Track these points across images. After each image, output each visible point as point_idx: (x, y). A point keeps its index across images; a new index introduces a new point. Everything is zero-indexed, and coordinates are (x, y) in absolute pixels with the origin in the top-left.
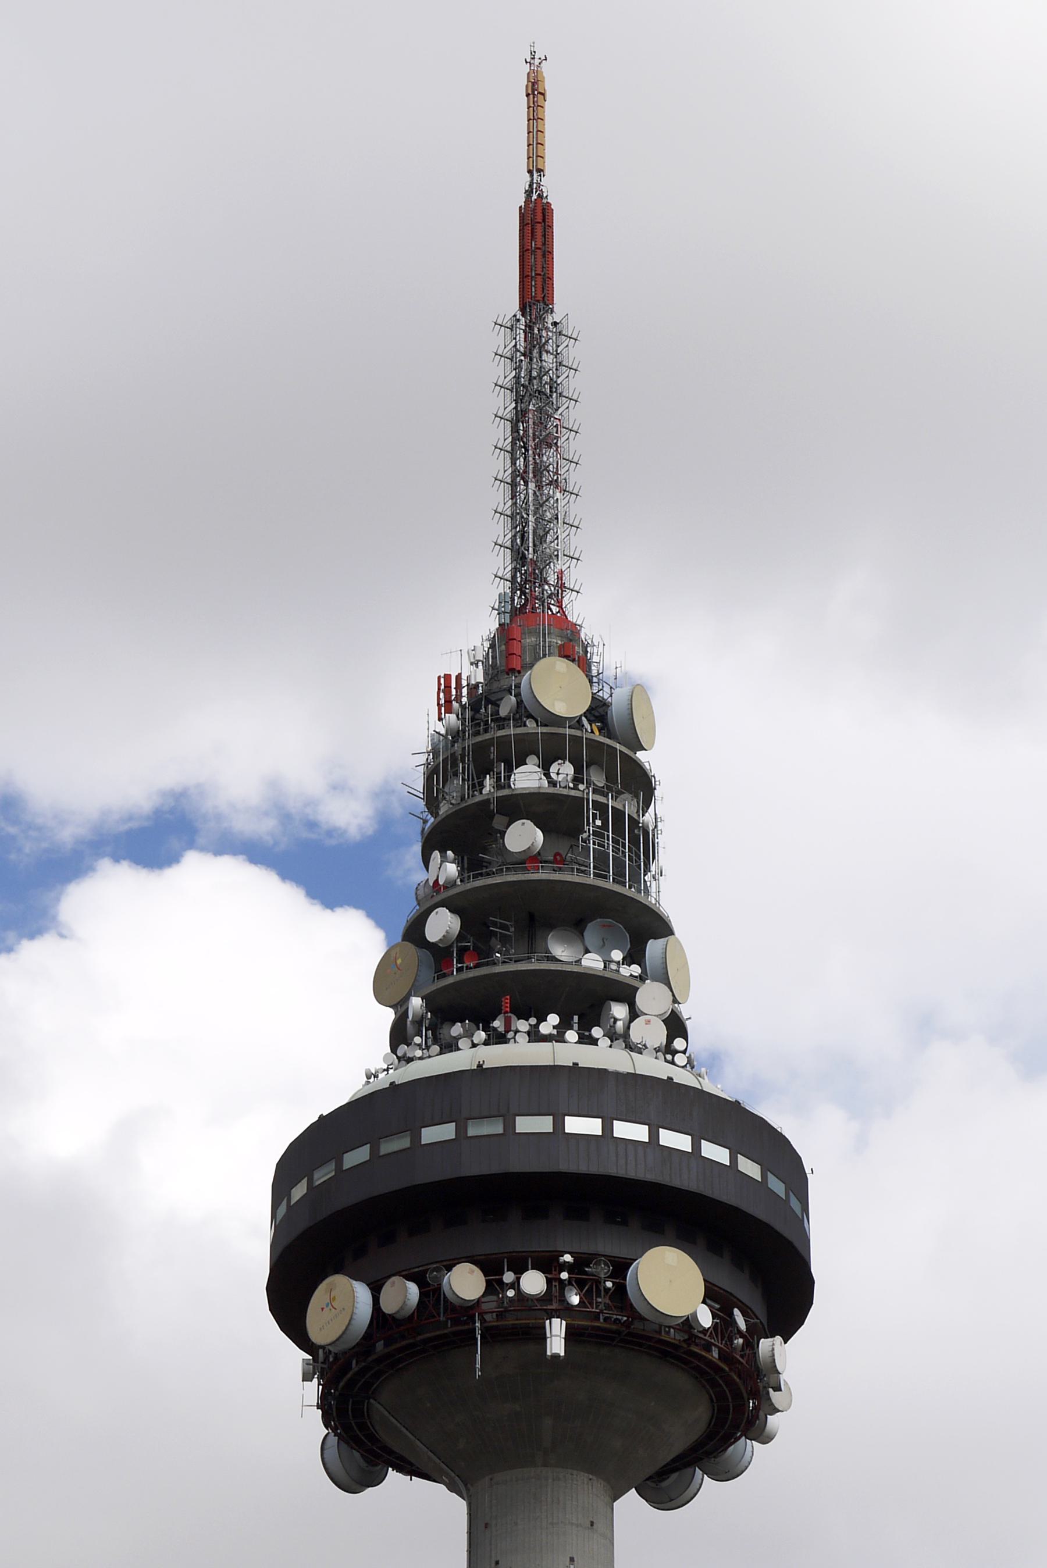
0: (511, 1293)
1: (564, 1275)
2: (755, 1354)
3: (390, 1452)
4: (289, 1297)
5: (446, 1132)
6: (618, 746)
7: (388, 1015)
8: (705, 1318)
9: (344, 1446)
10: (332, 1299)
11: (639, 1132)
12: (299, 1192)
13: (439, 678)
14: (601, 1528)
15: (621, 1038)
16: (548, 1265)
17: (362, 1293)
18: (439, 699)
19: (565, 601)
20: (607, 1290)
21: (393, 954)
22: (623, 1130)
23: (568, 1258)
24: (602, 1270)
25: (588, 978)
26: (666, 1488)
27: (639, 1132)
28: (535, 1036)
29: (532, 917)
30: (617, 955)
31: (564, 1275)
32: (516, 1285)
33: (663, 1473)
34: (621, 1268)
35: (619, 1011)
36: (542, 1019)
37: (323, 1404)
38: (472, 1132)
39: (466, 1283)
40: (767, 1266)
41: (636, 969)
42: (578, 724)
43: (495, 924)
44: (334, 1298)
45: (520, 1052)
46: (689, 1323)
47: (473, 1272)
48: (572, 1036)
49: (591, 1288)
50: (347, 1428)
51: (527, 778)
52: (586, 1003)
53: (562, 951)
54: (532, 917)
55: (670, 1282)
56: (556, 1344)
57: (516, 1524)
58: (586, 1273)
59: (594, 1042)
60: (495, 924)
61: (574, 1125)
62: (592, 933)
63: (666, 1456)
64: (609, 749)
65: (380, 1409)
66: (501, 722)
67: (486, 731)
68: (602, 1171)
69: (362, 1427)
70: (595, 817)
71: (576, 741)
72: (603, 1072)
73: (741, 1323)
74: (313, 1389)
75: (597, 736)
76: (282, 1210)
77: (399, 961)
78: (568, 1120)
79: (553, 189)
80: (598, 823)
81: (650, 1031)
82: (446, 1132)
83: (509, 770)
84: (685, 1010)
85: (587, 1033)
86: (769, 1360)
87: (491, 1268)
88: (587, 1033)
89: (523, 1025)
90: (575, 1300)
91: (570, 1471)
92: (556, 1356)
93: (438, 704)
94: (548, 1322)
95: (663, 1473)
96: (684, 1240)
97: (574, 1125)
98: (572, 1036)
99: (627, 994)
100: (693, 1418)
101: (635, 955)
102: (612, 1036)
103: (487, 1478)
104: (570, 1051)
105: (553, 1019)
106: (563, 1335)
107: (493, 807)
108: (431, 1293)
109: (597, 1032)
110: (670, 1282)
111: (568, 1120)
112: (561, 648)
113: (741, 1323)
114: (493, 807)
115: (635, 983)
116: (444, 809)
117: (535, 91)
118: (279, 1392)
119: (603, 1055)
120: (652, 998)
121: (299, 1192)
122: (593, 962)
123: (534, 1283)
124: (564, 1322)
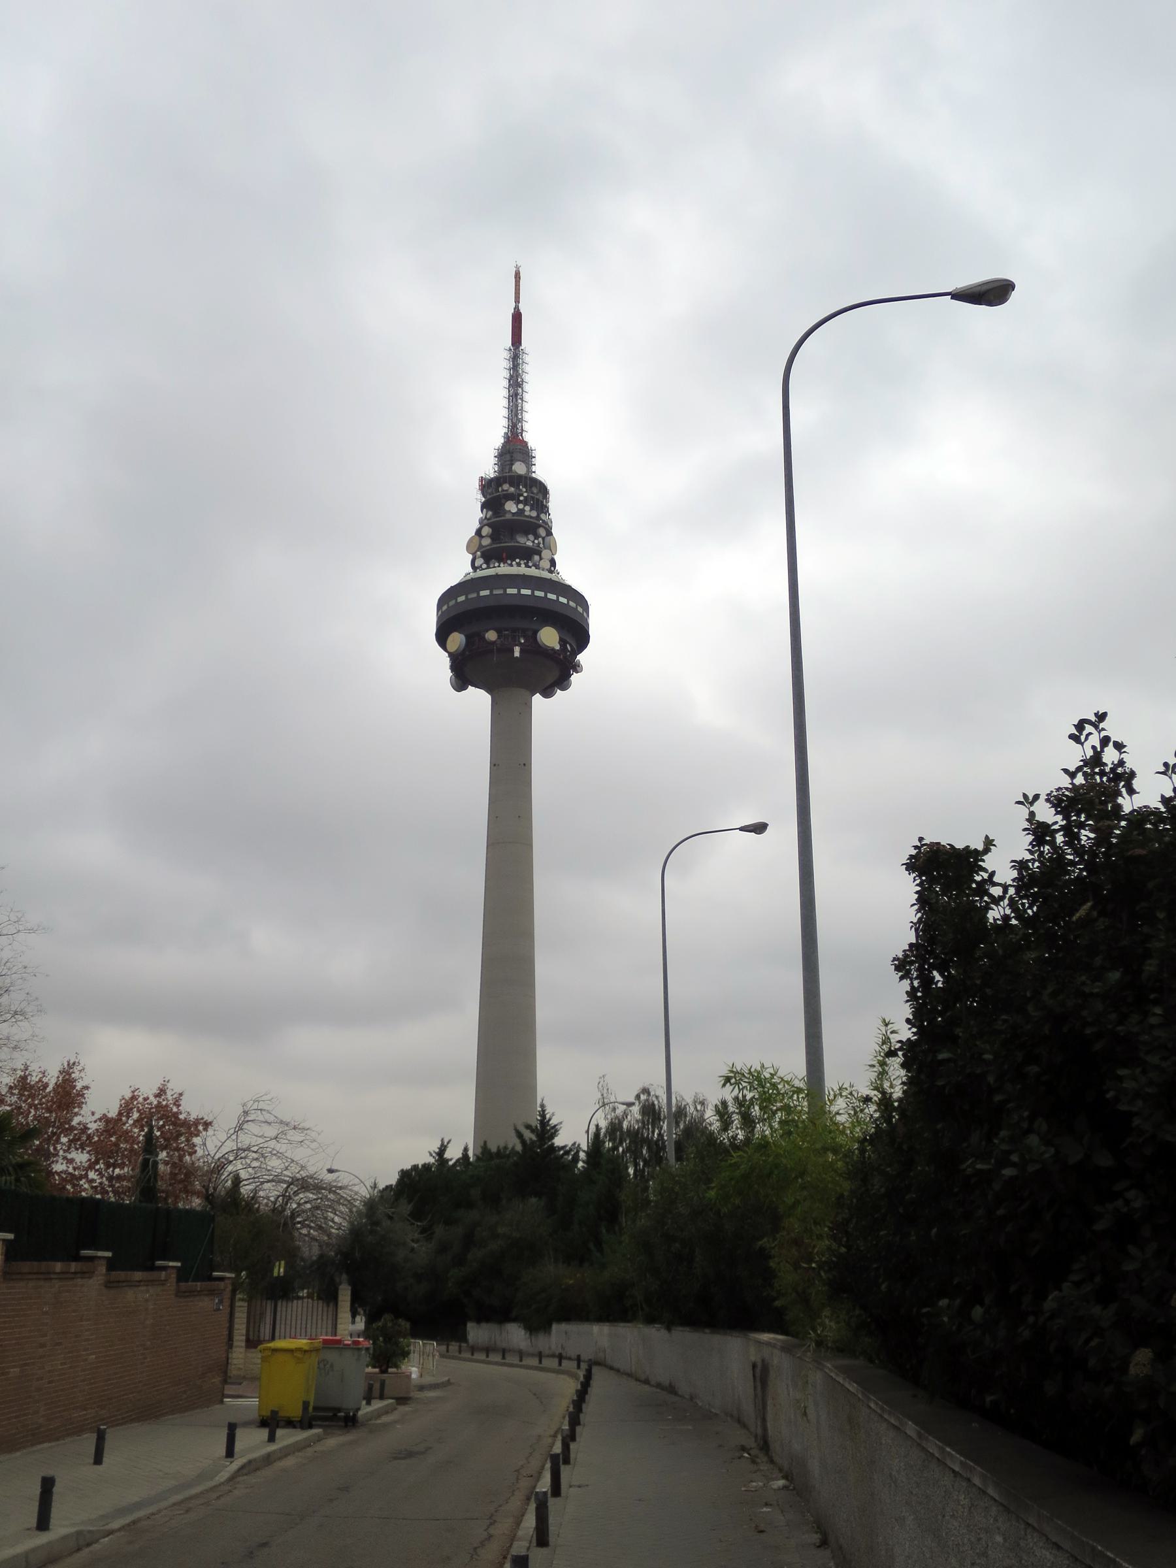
4: (442, 637)
7: (471, 557)
11: (528, 592)
12: (445, 608)
14: (528, 706)
15: (537, 567)
22: (523, 592)
25: (528, 548)
26: (547, 693)
27: (528, 592)
33: (546, 688)
34: (536, 632)
35: (536, 558)
40: (577, 633)
46: (553, 649)
52: (527, 555)
55: (549, 637)
56: (517, 653)
61: (509, 591)
64: (538, 493)
79: (532, 436)
81: (545, 564)
84: (556, 557)
95: (546, 688)
96: (553, 625)
97: (509, 591)
99: (539, 553)
100: (554, 675)
110: (549, 637)
117: (517, 276)
118: (441, 662)
120: (546, 554)
121: (445, 608)
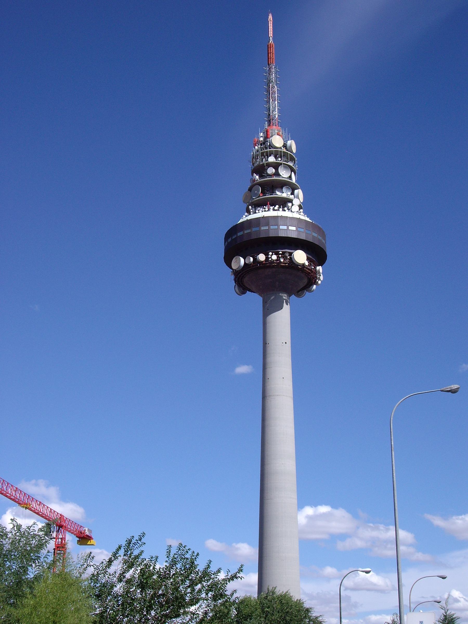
0: (270, 259)
1: (280, 256)
2: (316, 270)
3: (247, 287)
6: (289, 152)
8: (307, 264)
12: (229, 240)
16: (277, 254)
17: (242, 260)
23: (281, 252)
24: (287, 255)
29: (273, 186)
30: (289, 193)
31: (280, 256)
32: (271, 258)
34: (291, 254)
35: (290, 204)
36: (275, 206)
37: (235, 280)
39: (262, 257)
41: (293, 196)
42: (280, 148)
45: (271, 213)
46: (303, 265)
48: (281, 209)
50: (239, 284)
51: (272, 159)
53: (278, 194)
54: (273, 186)
55: (300, 257)
59: (285, 211)
62: (284, 189)
63: (299, 289)
65: (246, 280)
68: (287, 236)
69: (242, 284)
71: (281, 151)
72: (287, 217)
74: (233, 277)
75: (285, 150)
76: (226, 243)
83: (268, 157)
87: (267, 255)
89: (272, 208)
95: (298, 292)
98: (281, 209)
99: (291, 201)
100: (305, 281)
101: (293, 193)
102: (289, 209)
104: (280, 213)
105: (277, 206)
107: (265, 165)
108: (255, 259)
109: (286, 209)
110: (300, 257)
112: (278, 133)
114: (265, 165)
116: (255, 165)
119: (287, 214)
121: (229, 240)
122: (284, 195)
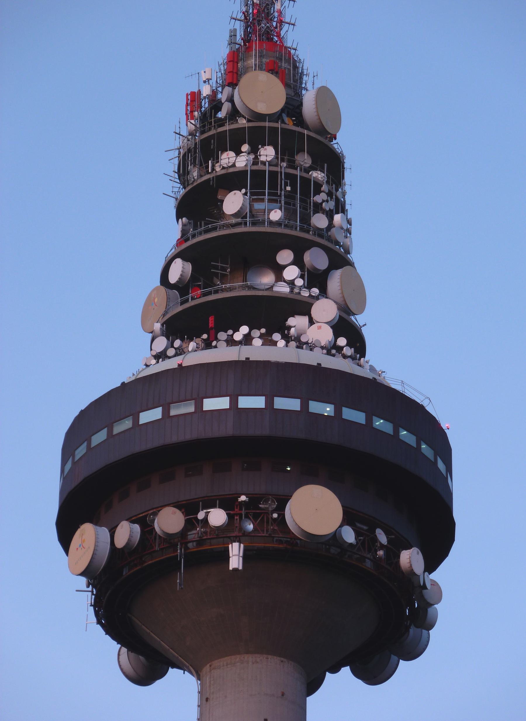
5: (156, 414)
6: (306, 132)
8: (349, 535)
9: (132, 655)
10: (83, 541)
11: (359, 417)
13: (187, 95)
16: (228, 504)
18: (187, 110)
19: (282, 33)
20: (275, 519)
21: (153, 296)
23: (243, 498)
25: (280, 299)
28: (231, 342)
36: (236, 330)
38: (173, 413)
43: (216, 267)
44: (84, 540)
47: (175, 513)
49: (263, 518)
55: (315, 510)
56: (235, 561)
57: (226, 697)
58: (260, 509)
60: (216, 267)
66: (221, 122)
67: (210, 129)
70: (286, 185)
73: (382, 538)
77: (156, 300)
78: (241, 399)
80: (289, 188)
82: (156, 414)
85: (270, 338)
86: (408, 565)
87: (189, 508)
88: (270, 338)
90: (250, 527)
91: (265, 656)
92: (235, 570)
93: (186, 114)
94: (230, 546)
102: (287, 338)
103: (208, 665)
105: (244, 329)
106: (241, 554)
110: (315, 510)
111: (241, 399)
113: (382, 538)
115: (310, 300)
119: (281, 352)
123: (217, 517)
124: (242, 545)
